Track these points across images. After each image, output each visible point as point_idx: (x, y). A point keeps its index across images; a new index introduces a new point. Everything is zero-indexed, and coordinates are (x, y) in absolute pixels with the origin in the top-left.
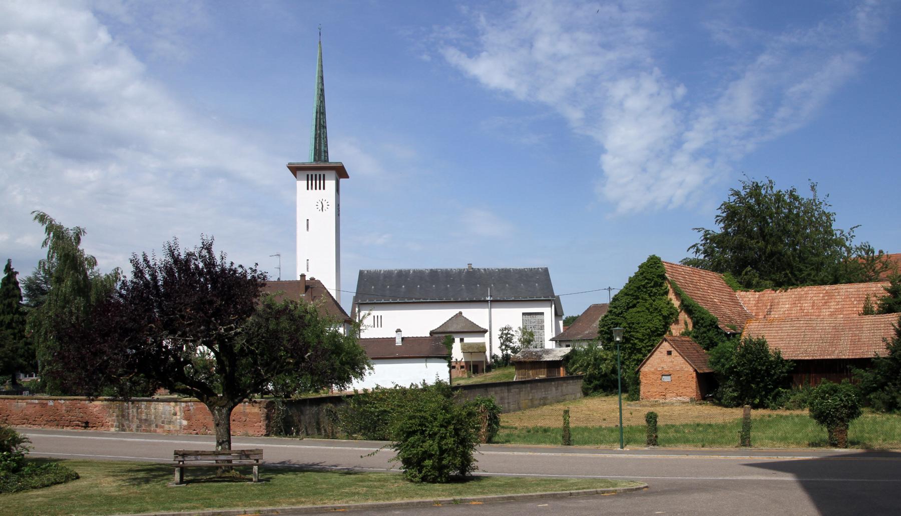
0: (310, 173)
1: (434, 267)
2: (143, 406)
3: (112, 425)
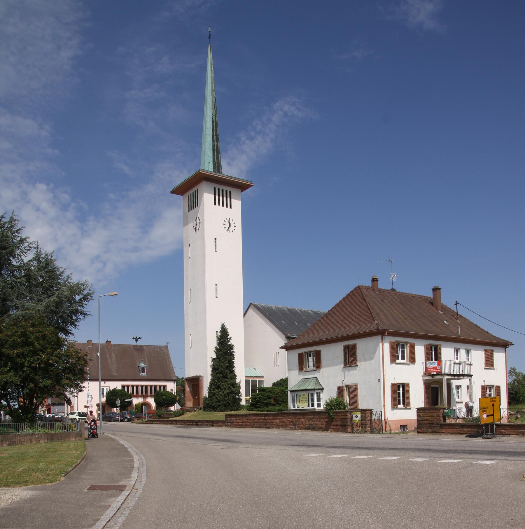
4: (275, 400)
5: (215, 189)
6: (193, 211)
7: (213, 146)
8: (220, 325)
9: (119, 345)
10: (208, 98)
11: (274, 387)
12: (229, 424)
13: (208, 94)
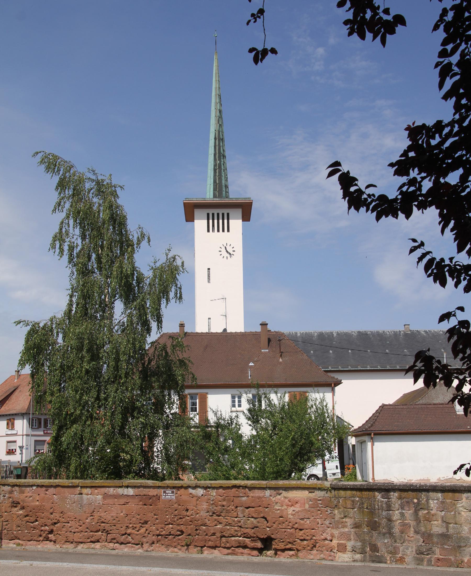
0: (211, 211)
1: (363, 328)
2: (433, 504)
3: (342, 548)
5: (208, 214)
7: (215, 166)
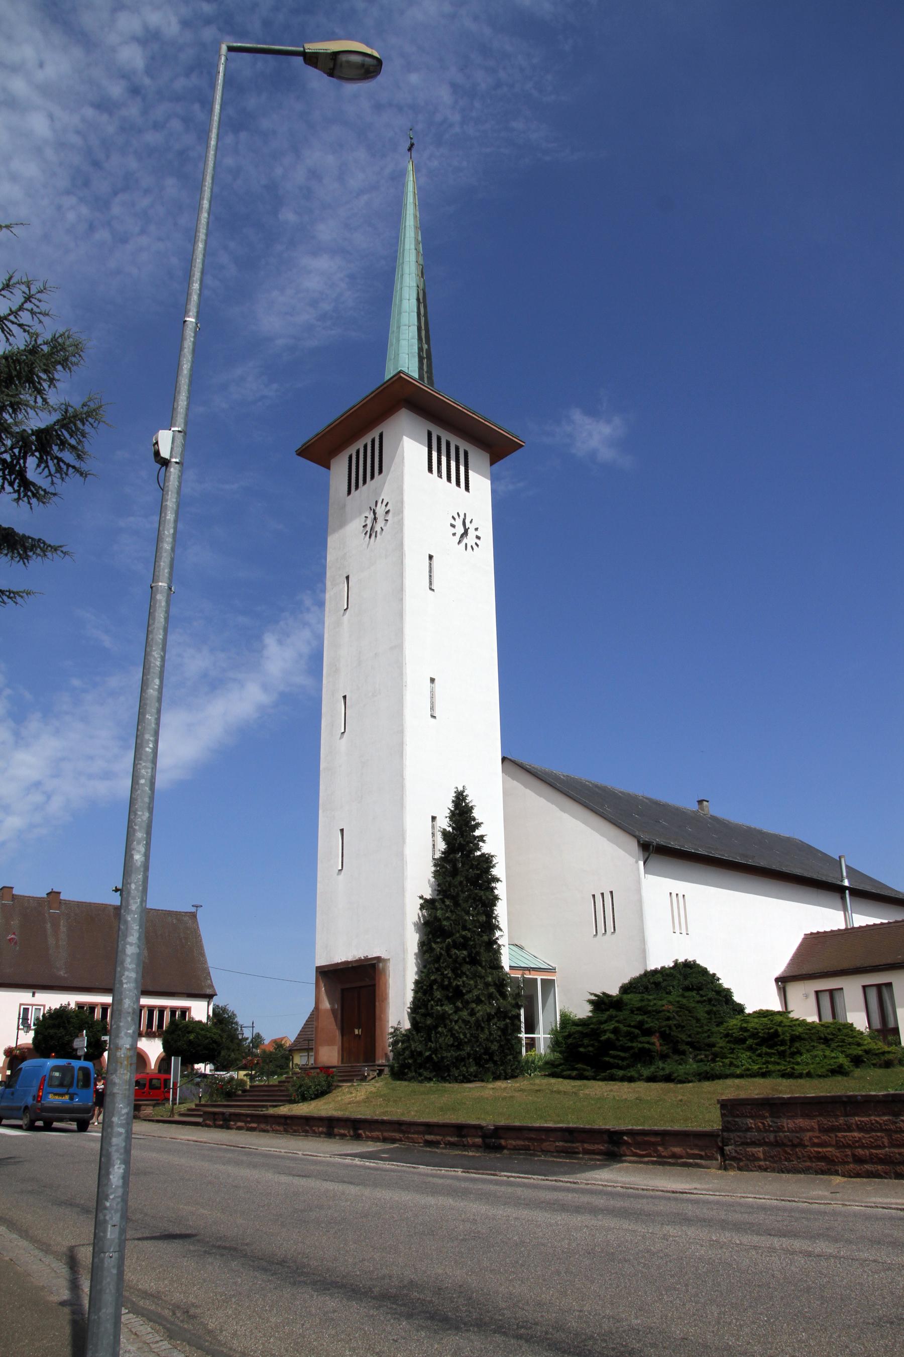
4: (665, 1037)
5: (430, 434)
6: (363, 489)
7: (420, 349)
8: (452, 796)
9: (80, 904)
10: (406, 254)
11: (625, 997)
12: (759, 1151)
13: (407, 247)
